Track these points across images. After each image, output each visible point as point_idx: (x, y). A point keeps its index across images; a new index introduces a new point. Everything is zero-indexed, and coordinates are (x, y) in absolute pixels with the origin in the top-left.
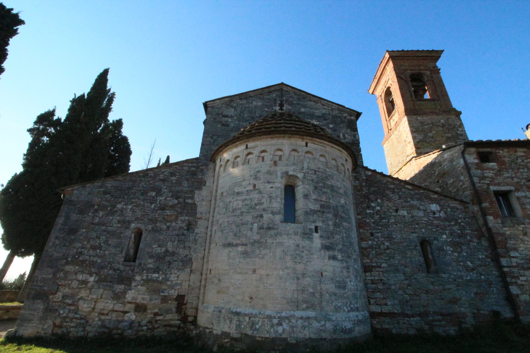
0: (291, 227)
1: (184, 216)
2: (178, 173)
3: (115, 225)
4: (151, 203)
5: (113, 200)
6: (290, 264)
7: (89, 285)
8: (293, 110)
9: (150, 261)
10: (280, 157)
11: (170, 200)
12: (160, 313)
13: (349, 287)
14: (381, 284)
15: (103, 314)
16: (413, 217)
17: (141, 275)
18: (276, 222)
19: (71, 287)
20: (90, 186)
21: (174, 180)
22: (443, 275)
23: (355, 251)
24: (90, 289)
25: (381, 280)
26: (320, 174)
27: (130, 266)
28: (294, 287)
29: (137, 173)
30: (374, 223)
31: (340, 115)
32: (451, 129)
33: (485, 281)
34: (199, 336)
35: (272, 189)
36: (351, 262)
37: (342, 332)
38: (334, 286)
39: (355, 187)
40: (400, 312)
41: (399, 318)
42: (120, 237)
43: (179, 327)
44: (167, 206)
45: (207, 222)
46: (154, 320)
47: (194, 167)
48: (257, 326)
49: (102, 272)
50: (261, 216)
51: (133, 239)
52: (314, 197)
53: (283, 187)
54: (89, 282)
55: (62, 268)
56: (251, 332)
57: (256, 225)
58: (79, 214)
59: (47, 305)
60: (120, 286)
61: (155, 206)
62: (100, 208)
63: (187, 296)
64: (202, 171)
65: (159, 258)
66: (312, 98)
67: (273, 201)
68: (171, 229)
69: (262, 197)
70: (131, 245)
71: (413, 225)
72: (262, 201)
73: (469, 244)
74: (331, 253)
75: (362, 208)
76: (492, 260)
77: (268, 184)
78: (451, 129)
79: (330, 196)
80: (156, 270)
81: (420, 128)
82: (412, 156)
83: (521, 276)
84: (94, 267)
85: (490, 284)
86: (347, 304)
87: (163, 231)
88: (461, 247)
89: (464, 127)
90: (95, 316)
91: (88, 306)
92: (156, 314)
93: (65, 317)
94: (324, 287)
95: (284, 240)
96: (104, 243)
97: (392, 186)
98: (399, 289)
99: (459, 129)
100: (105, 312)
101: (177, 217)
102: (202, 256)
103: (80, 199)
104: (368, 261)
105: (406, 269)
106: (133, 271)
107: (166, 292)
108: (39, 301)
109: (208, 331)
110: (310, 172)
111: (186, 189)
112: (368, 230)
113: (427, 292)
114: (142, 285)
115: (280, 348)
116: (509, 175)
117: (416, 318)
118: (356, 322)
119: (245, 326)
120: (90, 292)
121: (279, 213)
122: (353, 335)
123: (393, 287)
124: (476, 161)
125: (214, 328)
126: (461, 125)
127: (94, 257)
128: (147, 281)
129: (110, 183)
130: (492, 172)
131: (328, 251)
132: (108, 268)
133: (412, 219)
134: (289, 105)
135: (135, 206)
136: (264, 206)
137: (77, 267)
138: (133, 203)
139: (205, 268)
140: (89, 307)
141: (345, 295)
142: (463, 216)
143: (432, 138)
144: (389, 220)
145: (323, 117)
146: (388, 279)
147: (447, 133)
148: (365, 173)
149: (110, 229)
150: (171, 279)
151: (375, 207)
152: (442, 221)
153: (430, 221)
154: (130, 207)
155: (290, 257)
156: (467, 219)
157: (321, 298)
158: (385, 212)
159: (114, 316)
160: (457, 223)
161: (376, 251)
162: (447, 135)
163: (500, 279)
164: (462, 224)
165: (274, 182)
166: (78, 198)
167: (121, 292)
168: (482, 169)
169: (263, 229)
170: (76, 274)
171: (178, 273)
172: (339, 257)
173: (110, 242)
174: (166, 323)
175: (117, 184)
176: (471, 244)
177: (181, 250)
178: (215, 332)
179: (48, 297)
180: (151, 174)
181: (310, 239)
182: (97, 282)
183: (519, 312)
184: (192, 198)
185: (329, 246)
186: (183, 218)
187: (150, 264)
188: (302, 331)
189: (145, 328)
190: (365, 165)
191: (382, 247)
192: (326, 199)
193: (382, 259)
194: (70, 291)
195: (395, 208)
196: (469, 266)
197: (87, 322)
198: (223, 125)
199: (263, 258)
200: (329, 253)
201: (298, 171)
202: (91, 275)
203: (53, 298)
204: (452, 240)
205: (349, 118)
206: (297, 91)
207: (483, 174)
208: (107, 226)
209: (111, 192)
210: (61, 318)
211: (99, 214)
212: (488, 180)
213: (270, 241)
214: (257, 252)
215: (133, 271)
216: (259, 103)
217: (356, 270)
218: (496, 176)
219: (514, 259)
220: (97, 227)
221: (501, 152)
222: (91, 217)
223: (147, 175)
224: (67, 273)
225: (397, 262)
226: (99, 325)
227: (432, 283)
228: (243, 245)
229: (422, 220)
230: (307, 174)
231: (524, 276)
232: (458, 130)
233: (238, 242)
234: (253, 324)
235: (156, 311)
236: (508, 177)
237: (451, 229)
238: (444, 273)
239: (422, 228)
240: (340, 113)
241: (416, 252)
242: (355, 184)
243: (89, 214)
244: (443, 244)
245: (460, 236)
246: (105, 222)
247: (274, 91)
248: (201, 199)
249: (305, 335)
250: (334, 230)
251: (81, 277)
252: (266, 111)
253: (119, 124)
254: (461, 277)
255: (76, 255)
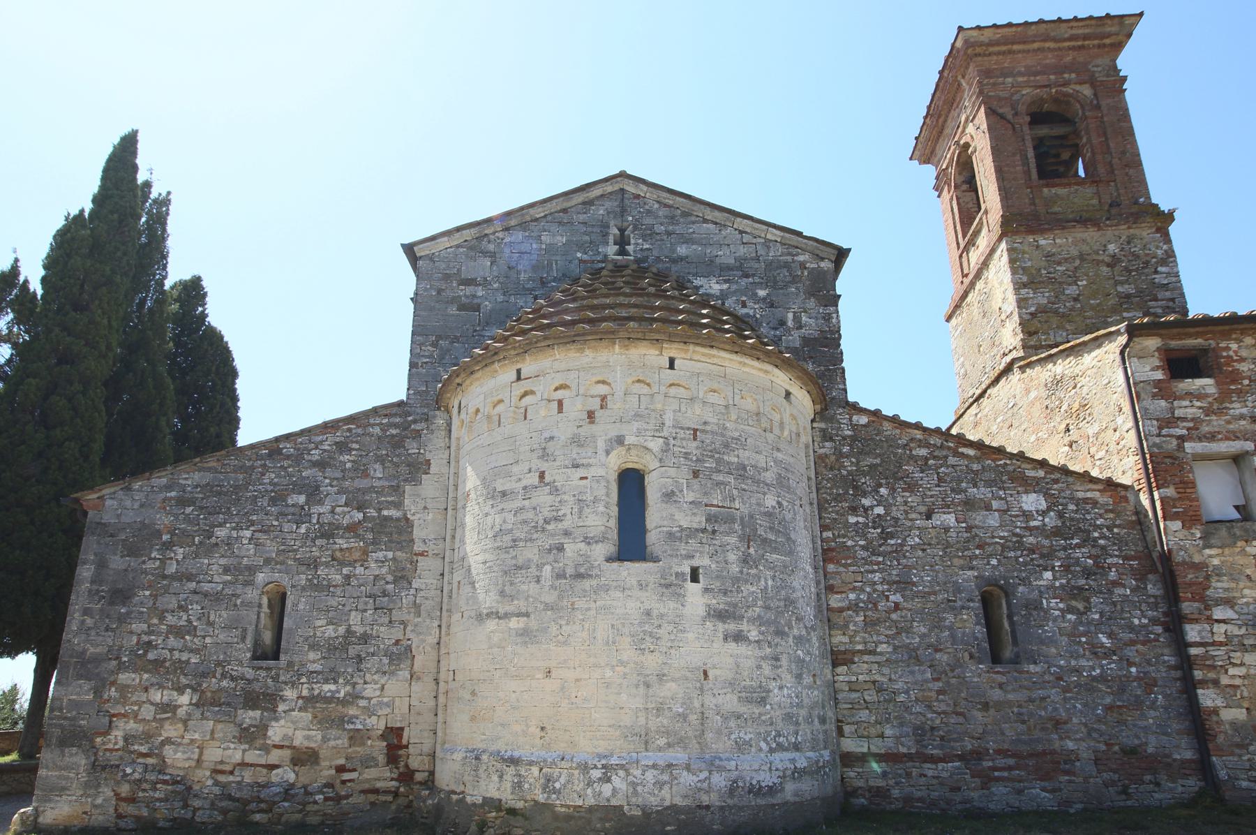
0: (632, 571)
1: (382, 550)
2: (357, 442)
3: (216, 579)
4: (298, 523)
5: (205, 518)
6: (628, 654)
7: (181, 712)
8: (655, 253)
9: (312, 655)
10: (602, 400)
11: (344, 514)
12: (349, 766)
13: (776, 699)
14: (873, 692)
15: (222, 772)
16: (969, 529)
17: (297, 688)
18: (596, 560)
19: (140, 717)
20: (141, 486)
21: (349, 461)
22: (1032, 668)
23: (799, 619)
24: (185, 722)
25: (874, 682)
26: (708, 439)
27: (268, 669)
28: (638, 703)
29: (252, 447)
30: (863, 548)
31: (789, 258)
32: (1137, 270)
33: (1138, 679)
34: (438, 810)
35: (584, 481)
36: (787, 645)
37: (750, 792)
38: (735, 698)
39: (820, 460)
40: (913, 751)
41: (910, 764)
42: (235, 605)
43: (396, 794)
44: (338, 528)
45: (439, 562)
46: (338, 781)
47: (395, 426)
48: (557, 785)
49: (205, 685)
50: (561, 548)
51: (265, 609)
52: (690, 497)
53: (613, 477)
54: (180, 706)
55: (112, 679)
56: (545, 795)
57: (548, 568)
58: (128, 556)
59: (93, 759)
60: (251, 713)
61: (308, 529)
62: (175, 538)
63: (406, 730)
64: (417, 435)
65: (334, 649)
66: (710, 216)
67: (587, 511)
68: (354, 582)
69: (560, 502)
70: (263, 621)
71: (970, 549)
72: (560, 513)
73: (1110, 592)
74: (732, 627)
75: (837, 512)
76: (1167, 630)
77: (574, 469)
78: (1137, 270)
79: (735, 492)
80: (332, 676)
81: (1044, 272)
82: (1014, 354)
83: (1234, 665)
84: (186, 675)
85: (1149, 684)
86: (769, 735)
87: (335, 586)
88: (1087, 600)
89: (1175, 261)
90: (203, 774)
91: (186, 756)
92: (341, 769)
93: (140, 780)
94: (710, 701)
95: (615, 603)
96: (199, 619)
97: (923, 452)
98: (917, 700)
99: (1159, 269)
100: (228, 768)
101: (365, 553)
102: (436, 641)
103: (124, 519)
104: (845, 639)
105: (938, 656)
106: (275, 679)
107: (358, 721)
108: (74, 750)
109: (455, 797)
110: (681, 434)
111: (381, 483)
112: (850, 565)
113: (986, 706)
114: (300, 710)
115: (607, 825)
116: (1244, 411)
117: (950, 764)
118: (789, 773)
119: (531, 785)
120: (186, 726)
121: (603, 539)
122: (778, 799)
123: (902, 698)
124: (1159, 375)
125: (467, 791)
126: (1169, 258)
127: (180, 651)
128: (310, 701)
129: (191, 477)
130: (1198, 404)
131: (724, 622)
132: (218, 676)
133: (966, 535)
134: (644, 237)
135: (260, 531)
136: (566, 524)
137: (146, 676)
138: (253, 523)
139: (443, 669)
140: (189, 759)
141: (763, 718)
142: (1109, 523)
143: (1076, 300)
144: (904, 540)
145: (740, 268)
146: (890, 680)
147: (1122, 283)
148: (850, 419)
149: (206, 587)
150: (367, 693)
151: (872, 507)
152: (1047, 537)
153: (1014, 539)
154: (248, 534)
155: (629, 639)
156: (1116, 530)
157: (702, 724)
158: (896, 520)
159: (248, 776)
160: (1087, 540)
161: (865, 616)
162: (1120, 289)
163: (1178, 674)
164: (1102, 542)
165: (589, 465)
166: (119, 516)
167: (254, 726)
168: (1171, 396)
169: (566, 578)
170: (146, 690)
171: (383, 681)
172: (753, 634)
173: (212, 618)
174: (367, 786)
175: (207, 477)
176: (1119, 591)
177: (382, 629)
178: (469, 799)
179: (92, 741)
180: (288, 448)
181: (680, 597)
182: (197, 705)
183: (1211, 746)
184: (398, 505)
185: (727, 611)
186: (380, 555)
187: (314, 662)
188: (656, 792)
189: (319, 797)
190: (851, 398)
191: (882, 605)
192: (724, 500)
193: (878, 634)
194: (141, 728)
195: (923, 509)
196: (1102, 645)
197: (190, 788)
198: (462, 307)
199: (565, 643)
200: (726, 626)
201: (649, 433)
202: (181, 690)
203: (104, 744)
204: (1068, 583)
205: (813, 266)
206: (665, 195)
207: (1172, 410)
208: (199, 582)
209: (197, 498)
210: (129, 782)
211: (176, 554)
212: (1184, 427)
213: (580, 604)
214: (554, 629)
215: (275, 679)
216: (559, 238)
217: (800, 661)
218: (1207, 415)
219: (1222, 624)
220: (176, 584)
221: (1234, 346)
222: (158, 563)
223: (279, 451)
224: (123, 689)
225: (917, 640)
226: (216, 795)
227: (1001, 686)
228: (519, 615)
229: (993, 537)
230: (672, 442)
231: (1242, 664)
232: (1156, 272)
233: (509, 608)
234: (549, 780)
235: (342, 761)
236: (1242, 417)
237: (1068, 557)
238: (1035, 663)
239: (990, 556)
240: (790, 254)
241: (968, 614)
242: (822, 451)
243: (153, 556)
244: (1040, 592)
245: (1087, 573)
246: (194, 571)
247: (598, 198)
248: (421, 506)
249: (663, 800)
250: (741, 572)
251: (160, 695)
252: (581, 261)
253: (193, 291)
254: (1077, 671)
255: (139, 650)
